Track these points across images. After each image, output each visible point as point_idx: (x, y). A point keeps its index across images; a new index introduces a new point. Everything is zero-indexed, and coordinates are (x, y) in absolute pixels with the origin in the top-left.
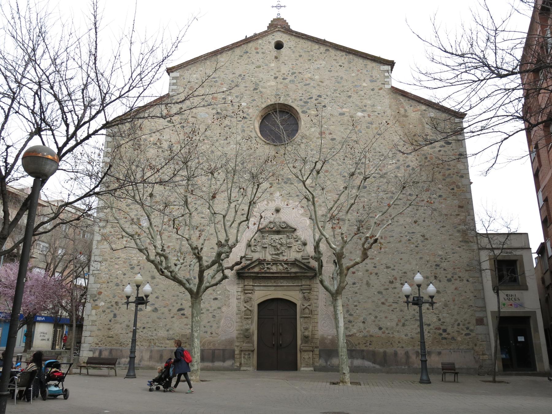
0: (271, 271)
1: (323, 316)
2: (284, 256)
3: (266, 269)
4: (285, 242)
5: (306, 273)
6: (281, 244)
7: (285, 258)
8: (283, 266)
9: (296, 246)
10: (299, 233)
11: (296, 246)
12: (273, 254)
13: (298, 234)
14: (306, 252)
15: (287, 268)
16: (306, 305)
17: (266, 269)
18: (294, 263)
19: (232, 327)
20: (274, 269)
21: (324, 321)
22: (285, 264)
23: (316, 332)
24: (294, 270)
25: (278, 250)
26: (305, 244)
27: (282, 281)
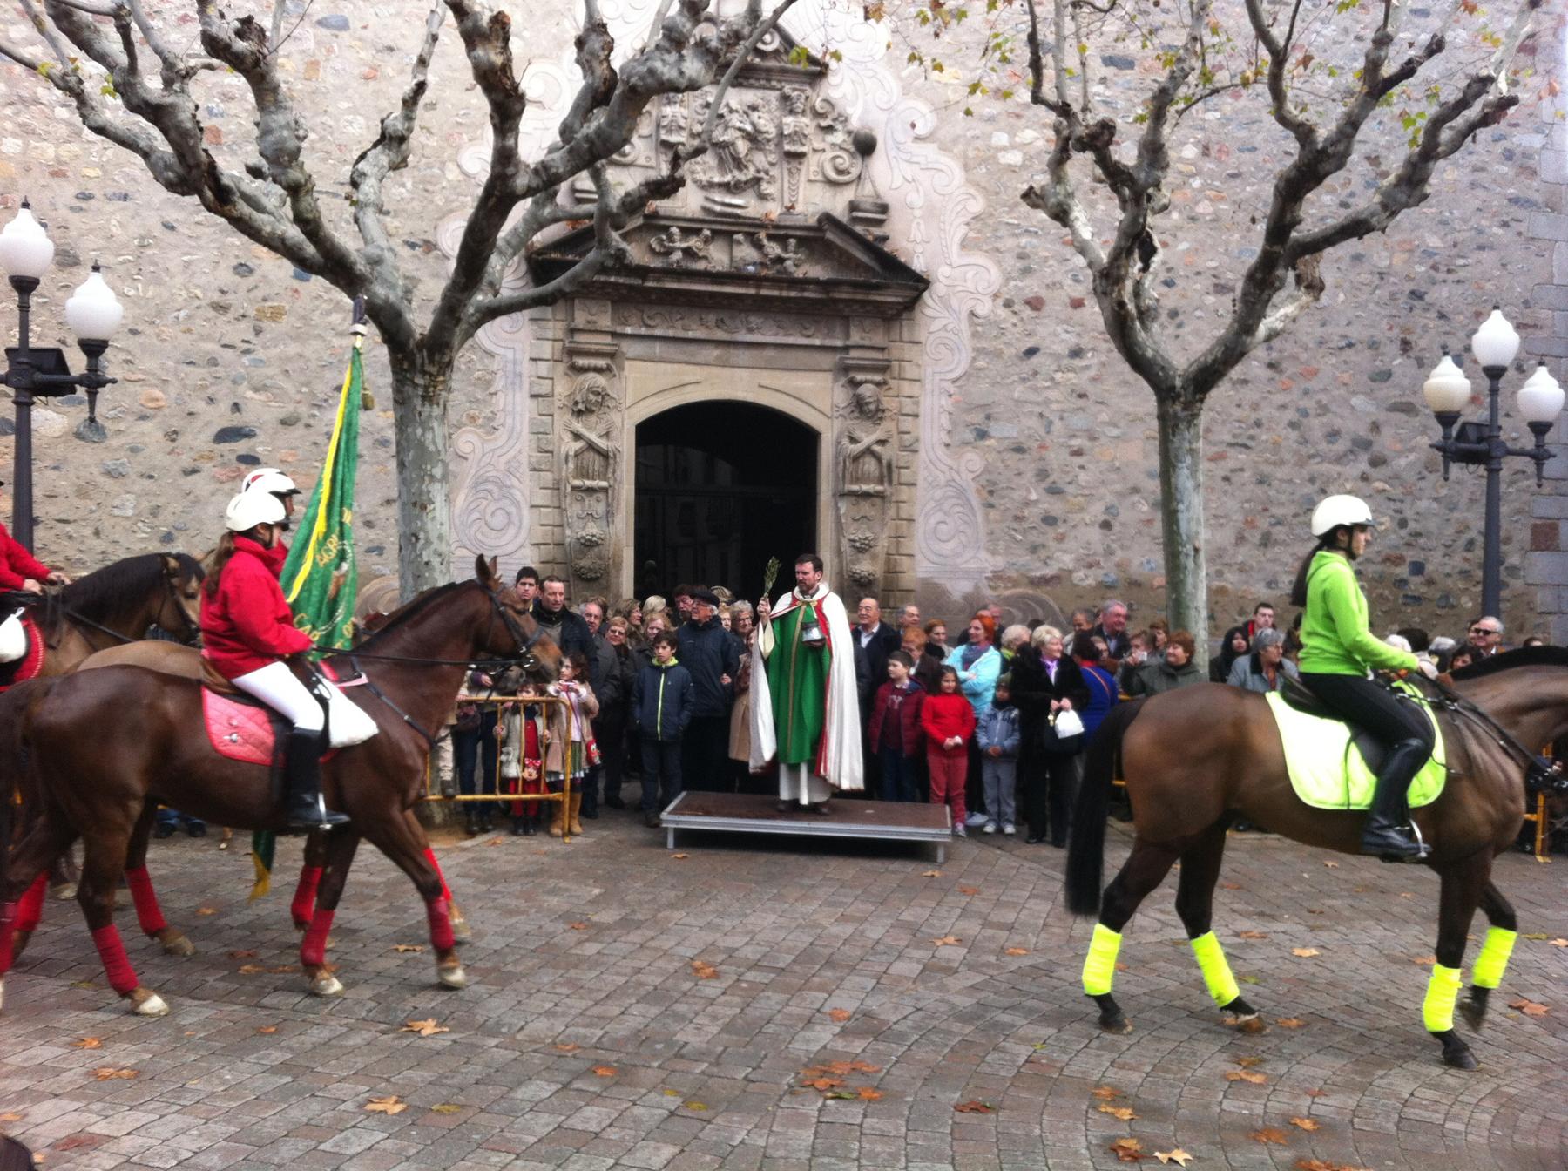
0: (700, 266)
1: (938, 494)
2: (763, 197)
3: (678, 255)
4: (772, 131)
5: (877, 287)
6: (754, 138)
7: (774, 210)
8: (758, 246)
9: (825, 153)
10: (839, 87)
11: (825, 153)
12: (711, 185)
13: (834, 94)
14: (868, 189)
15: (780, 260)
16: (867, 440)
17: (678, 255)
18: (818, 237)
19: (512, 531)
20: (718, 257)
21: (939, 516)
22: (771, 237)
23: (905, 562)
24: (816, 271)
25: (739, 164)
26: (865, 146)
27: (755, 320)
